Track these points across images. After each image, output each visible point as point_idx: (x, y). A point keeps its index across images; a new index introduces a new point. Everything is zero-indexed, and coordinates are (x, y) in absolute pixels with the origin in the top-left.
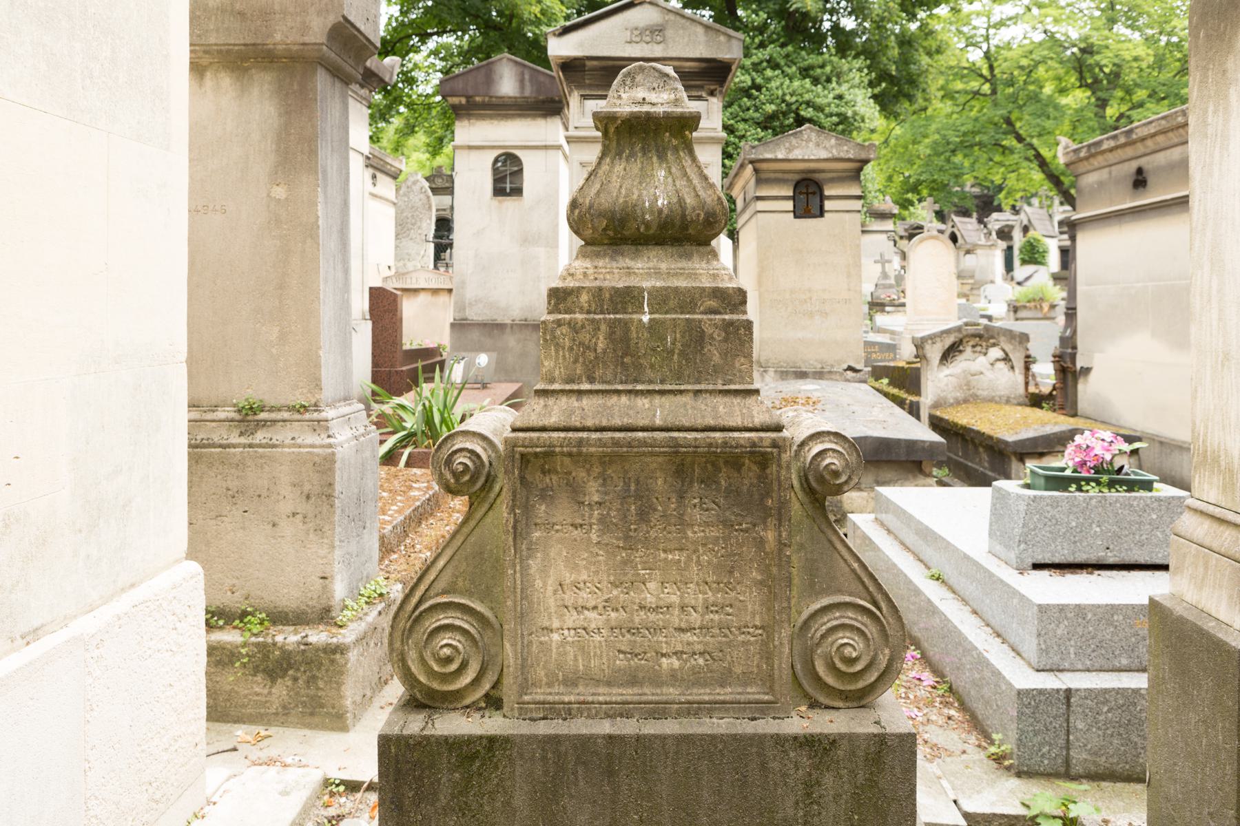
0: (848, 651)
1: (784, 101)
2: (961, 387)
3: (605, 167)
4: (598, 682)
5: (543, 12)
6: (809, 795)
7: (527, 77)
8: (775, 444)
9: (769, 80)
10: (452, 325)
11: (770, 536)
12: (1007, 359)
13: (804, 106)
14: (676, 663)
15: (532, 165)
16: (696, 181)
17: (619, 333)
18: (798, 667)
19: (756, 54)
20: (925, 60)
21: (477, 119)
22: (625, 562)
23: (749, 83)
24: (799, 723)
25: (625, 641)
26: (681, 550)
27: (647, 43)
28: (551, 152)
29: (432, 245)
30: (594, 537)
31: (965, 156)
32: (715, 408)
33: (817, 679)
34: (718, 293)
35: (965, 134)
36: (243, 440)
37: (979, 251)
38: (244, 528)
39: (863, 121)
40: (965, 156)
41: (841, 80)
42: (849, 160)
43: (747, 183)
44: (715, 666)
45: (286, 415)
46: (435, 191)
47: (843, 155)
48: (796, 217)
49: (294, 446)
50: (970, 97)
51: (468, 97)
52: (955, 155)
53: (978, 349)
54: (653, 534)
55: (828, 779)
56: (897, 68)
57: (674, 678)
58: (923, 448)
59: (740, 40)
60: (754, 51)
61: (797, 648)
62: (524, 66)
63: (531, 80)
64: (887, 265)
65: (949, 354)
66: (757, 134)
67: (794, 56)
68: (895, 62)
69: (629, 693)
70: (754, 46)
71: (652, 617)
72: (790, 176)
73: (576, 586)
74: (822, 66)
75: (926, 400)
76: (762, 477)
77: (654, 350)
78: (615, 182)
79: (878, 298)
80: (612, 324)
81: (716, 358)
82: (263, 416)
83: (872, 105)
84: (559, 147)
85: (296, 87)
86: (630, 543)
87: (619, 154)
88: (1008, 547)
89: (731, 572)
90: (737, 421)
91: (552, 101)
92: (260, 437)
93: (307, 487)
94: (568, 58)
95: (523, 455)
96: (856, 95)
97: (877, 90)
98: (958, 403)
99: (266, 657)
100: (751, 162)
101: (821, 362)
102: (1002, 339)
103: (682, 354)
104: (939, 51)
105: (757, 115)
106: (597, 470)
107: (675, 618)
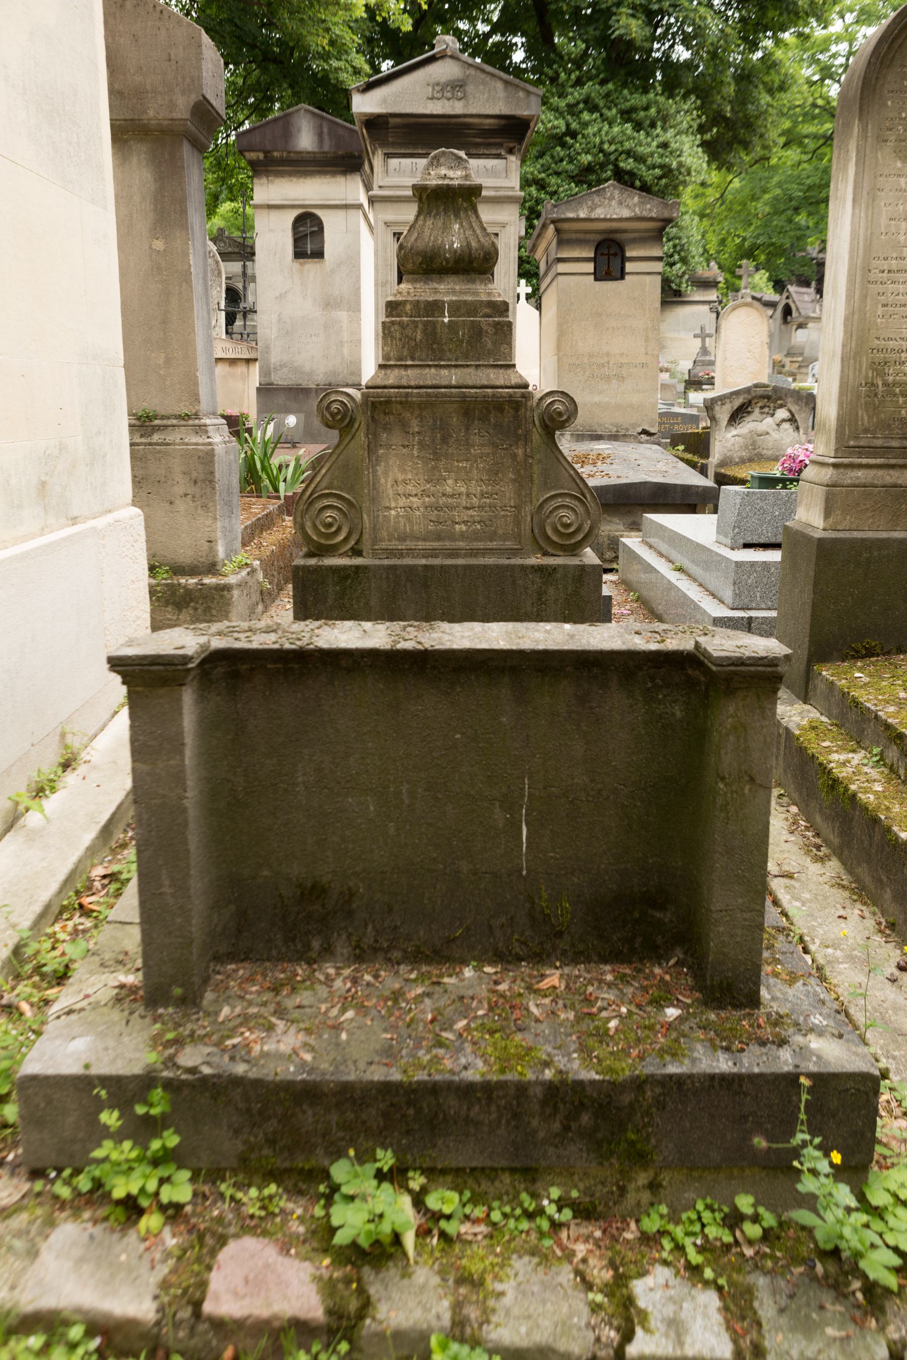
0: (565, 519)
1: (601, 150)
2: (746, 447)
3: (420, 222)
4: (418, 539)
5: (332, 43)
6: (540, 599)
7: (325, 130)
8: (523, 396)
9: (586, 125)
10: (258, 389)
11: (520, 452)
12: (792, 420)
13: (623, 156)
14: (464, 528)
15: (332, 222)
16: (478, 232)
17: (429, 328)
18: (536, 531)
19: (572, 94)
20: (765, 99)
21: (276, 176)
22: (434, 468)
23: (564, 129)
24: (535, 560)
25: (434, 515)
26: (467, 460)
27: (449, 99)
28: (352, 212)
29: (223, 313)
30: (415, 453)
31: (810, 214)
32: (488, 376)
33: (548, 538)
34: (492, 304)
35: (810, 188)
36: (143, 440)
37: (810, 325)
38: (148, 505)
39: (689, 174)
40: (810, 214)
41: (667, 125)
42: (651, 219)
43: (549, 244)
44: (487, 529)
45: (174, 422)
46: (226, 256)
47: (645, 214)
48: (596, 279)
49: (183, 444)
50: (821, 141)
51: (266, 153)
52: (799, 214)
53: (766, 410)
54: (450, 451)
55: (551, 591)
56: (732, 109)
57: (463, 536)
58: (697, 493)
59: (538, 95)
60: (570, 90)
61: (535, 520)
62: (322, 118)
63: (330, 134)
64: (707, 339)
65: (737, 416)
66: (571, 189)
67: (615, 96)
68: (730, 102)
69: (436, 544)
70: (570, 83)
71: (450, 500)
72: (592, 237)
73: (405, 482)
74: (646, 108)
75: (714, 459)
76: (516, 417)
77: (451, 340)
78: (427, 232)
79: (696, 376)
80: (426, 324)
81: (490, 345)
82: (157, 422)
83: (700, 154)
84: (360, 206)
85: (167, 157)
86: (437, 457)
87: (429, 213)
88: (726, 537)
89: (497, 474)
90: (501, 382)
91: (352, 156)
92: (156, 438)
93: (194, 475)
94: (371, 114)
95: (373, 403)
96: (682, 143)
97: (707, 137)
98: (743, 461)
99: (174, 594)
100: (553, 222)
101: (616, 426)
102: (789, 400)
103: (468, 342)
104: (783, 88)
105: (571, 167)
106: (417, 412)
107: (464, 501)
